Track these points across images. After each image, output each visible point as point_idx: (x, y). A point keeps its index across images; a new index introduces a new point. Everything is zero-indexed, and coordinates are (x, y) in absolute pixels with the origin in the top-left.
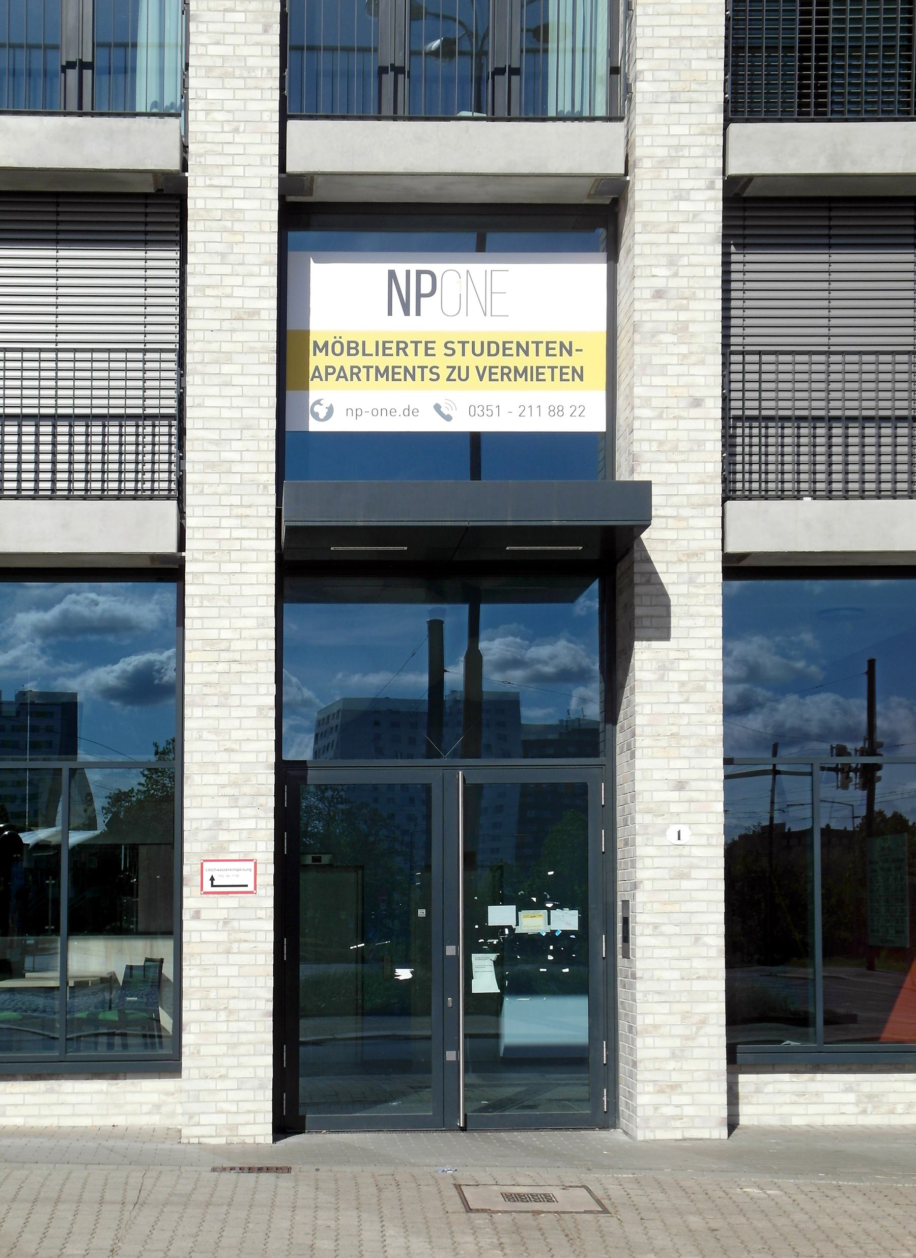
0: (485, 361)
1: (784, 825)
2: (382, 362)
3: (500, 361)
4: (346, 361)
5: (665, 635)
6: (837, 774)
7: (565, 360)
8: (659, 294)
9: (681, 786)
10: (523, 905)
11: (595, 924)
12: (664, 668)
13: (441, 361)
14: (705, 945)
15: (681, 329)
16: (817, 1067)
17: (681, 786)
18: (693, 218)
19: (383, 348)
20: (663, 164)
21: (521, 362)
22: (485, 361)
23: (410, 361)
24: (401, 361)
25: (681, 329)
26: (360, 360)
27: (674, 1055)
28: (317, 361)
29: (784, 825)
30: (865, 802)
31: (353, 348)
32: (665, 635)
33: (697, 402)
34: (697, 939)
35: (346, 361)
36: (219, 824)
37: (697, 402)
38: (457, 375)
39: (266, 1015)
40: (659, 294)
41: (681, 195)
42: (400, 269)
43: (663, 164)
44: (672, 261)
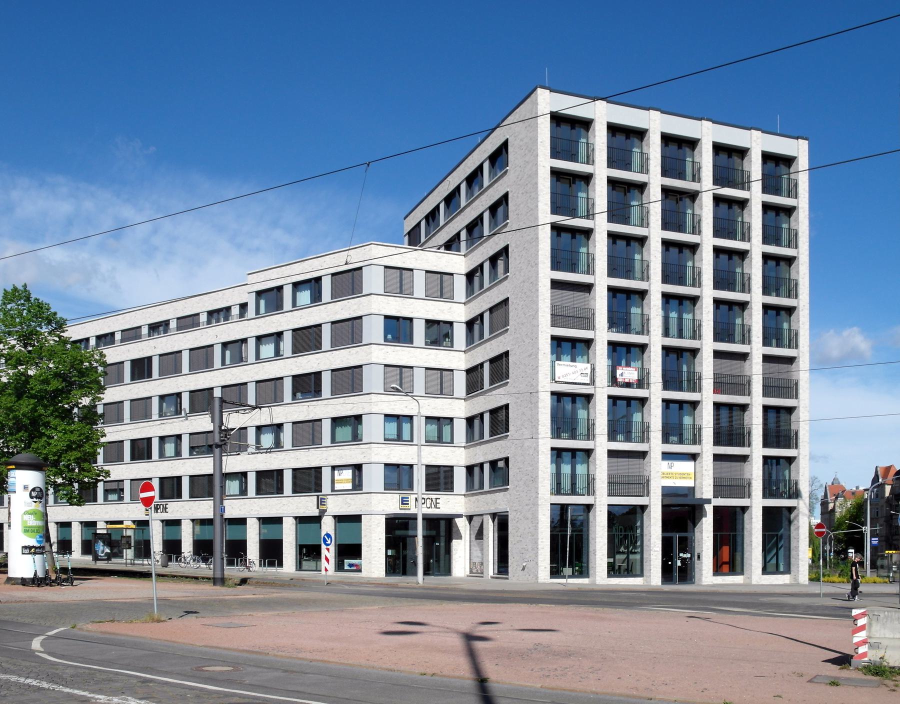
0: (680, 476)
2: (667, 476)
3: (681, 476)
5: (706, 517)
6: (97, 405)
7: (689, 476)
8: (706, 470)
9: (708, 537)
10: (684, 553)
11: (693, 556)
12: (706, 521)
13: (674, 476)
14: (116, 490)
16: (717, 576)
17: (708, 537)
18: (710, 460)
19: (667, 474)
20: (706, 452)
21: (684, 476)
22: (680, 476)
23: (670, 476)
26: (664, 475)
27: (707, 573)
32: (706, 517)
33: (710, 485)
36: (655, 542)
37: (710, 485)
39: (257, 543)
40: (706, 470)
41: (708, 457)
42: (669, 462)
43: (706, 452)
44: (707, 465)
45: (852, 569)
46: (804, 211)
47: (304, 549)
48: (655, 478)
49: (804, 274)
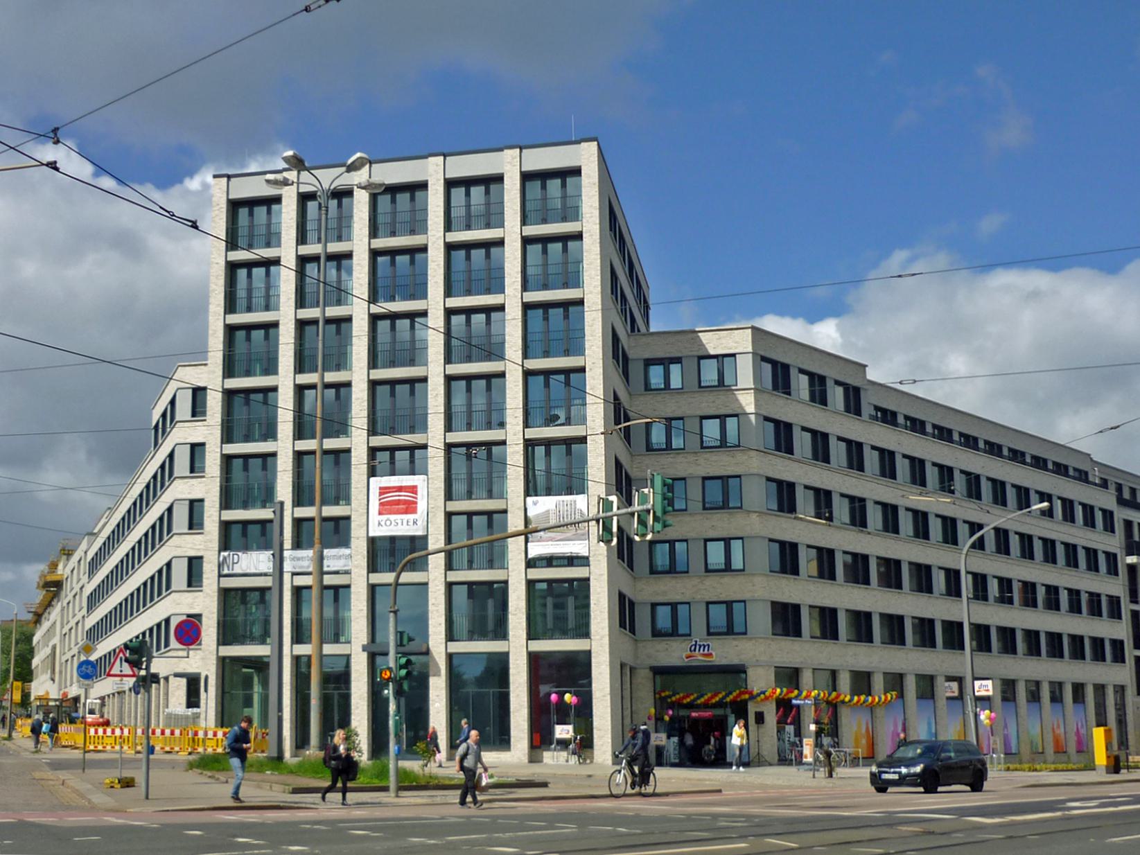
15: (437, 611)
25: (437, 611)
46: (591, 235)
48: (357, 618)
49: (594, 320)
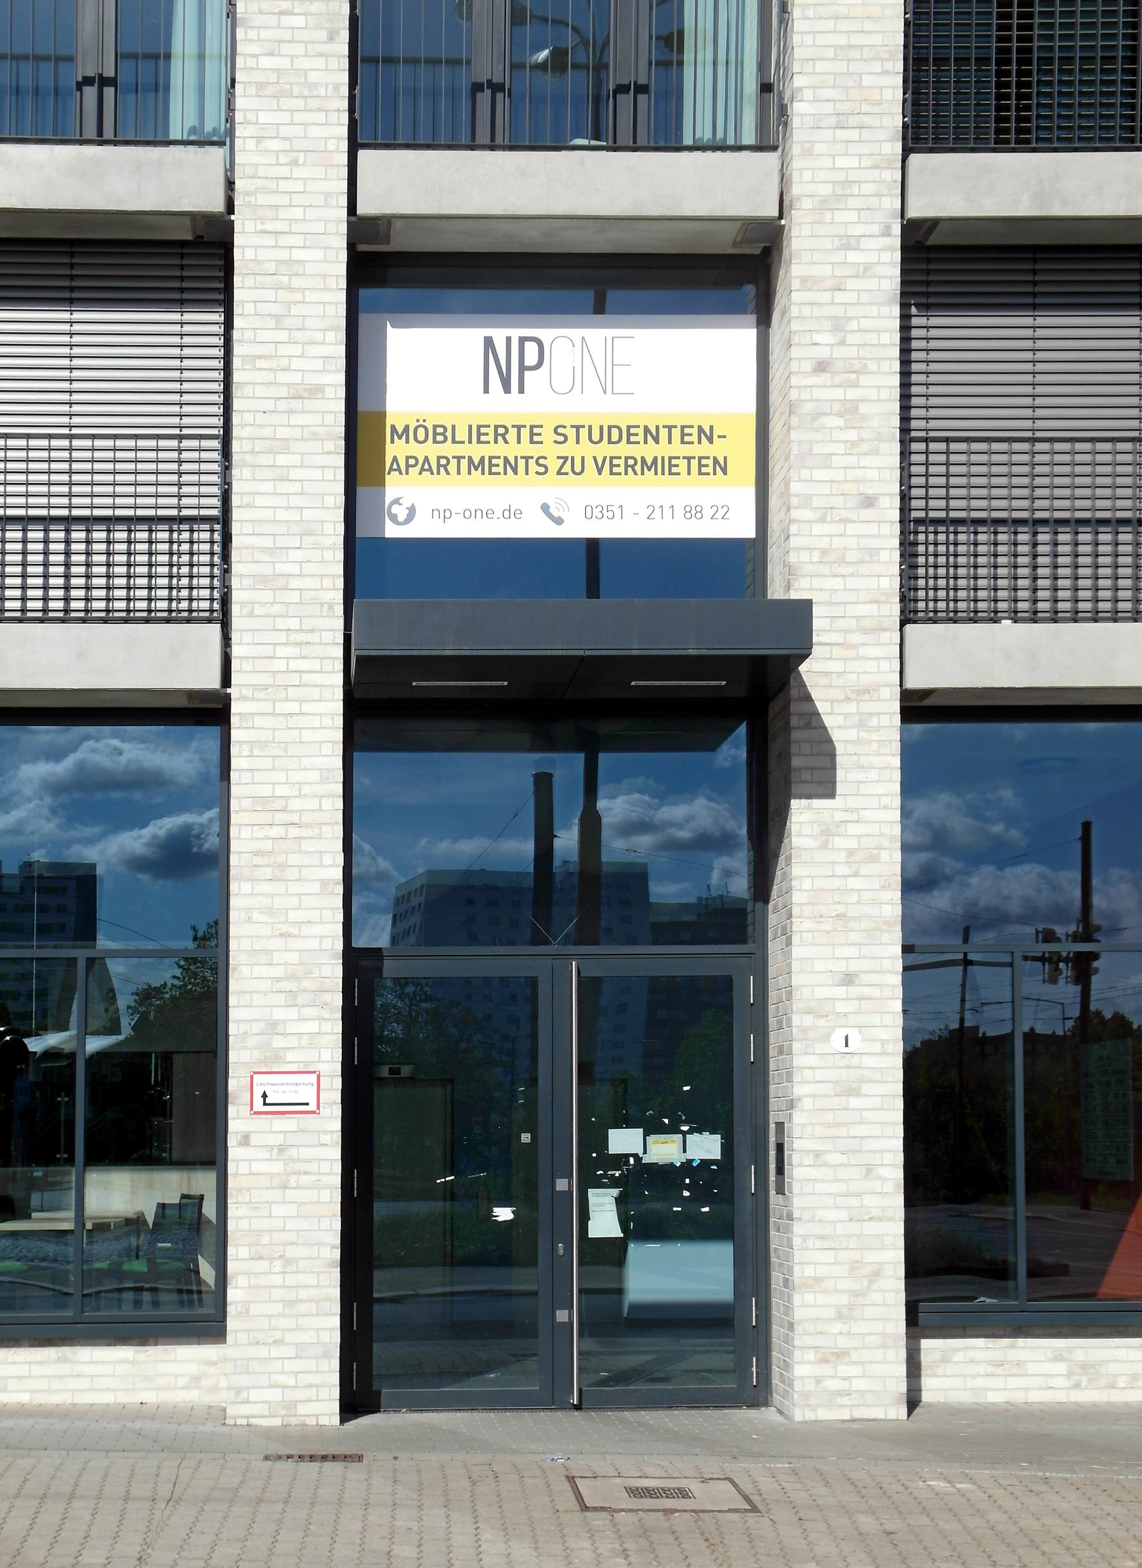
0: (604, 450)
1: (977, 1028)
2: (476, 451)
3: (623, 449)
4: (431, 450)
5: (829, 791)
7: (704, 449)
8: (821, 367)
9: (849, 979)
10: (652, 1128)
11: (742, 1151)
12: (828, 833)
13: (550, 450)
15: (850, 410)
16: (1019, 1330)
17: (849, 979)
18: (864, 272)
19: (477, 434)
20: (826, 205)
21: (650, 451)
22: (604, 450)
23: (511, 450)
24: (500, 449)
25: (850, 410)
26: (449, 449)
27: (841, 1315)
28: (395, 450)
29: (977, 1028)
30: (1078, 1000)
31: (440, 433)
32: (829, 791)
33: (869, 502)
34: (869, 1170)
35: (431, 450)
36: (273, 1027)
37: (869, 502)
38: (570, 467)
40: (821, 367)
41: (849, 243)
42: (499, 335)
43: (826, 205)
44: (838, 325)
45: (275, 1416)
47: (680, 1209)
